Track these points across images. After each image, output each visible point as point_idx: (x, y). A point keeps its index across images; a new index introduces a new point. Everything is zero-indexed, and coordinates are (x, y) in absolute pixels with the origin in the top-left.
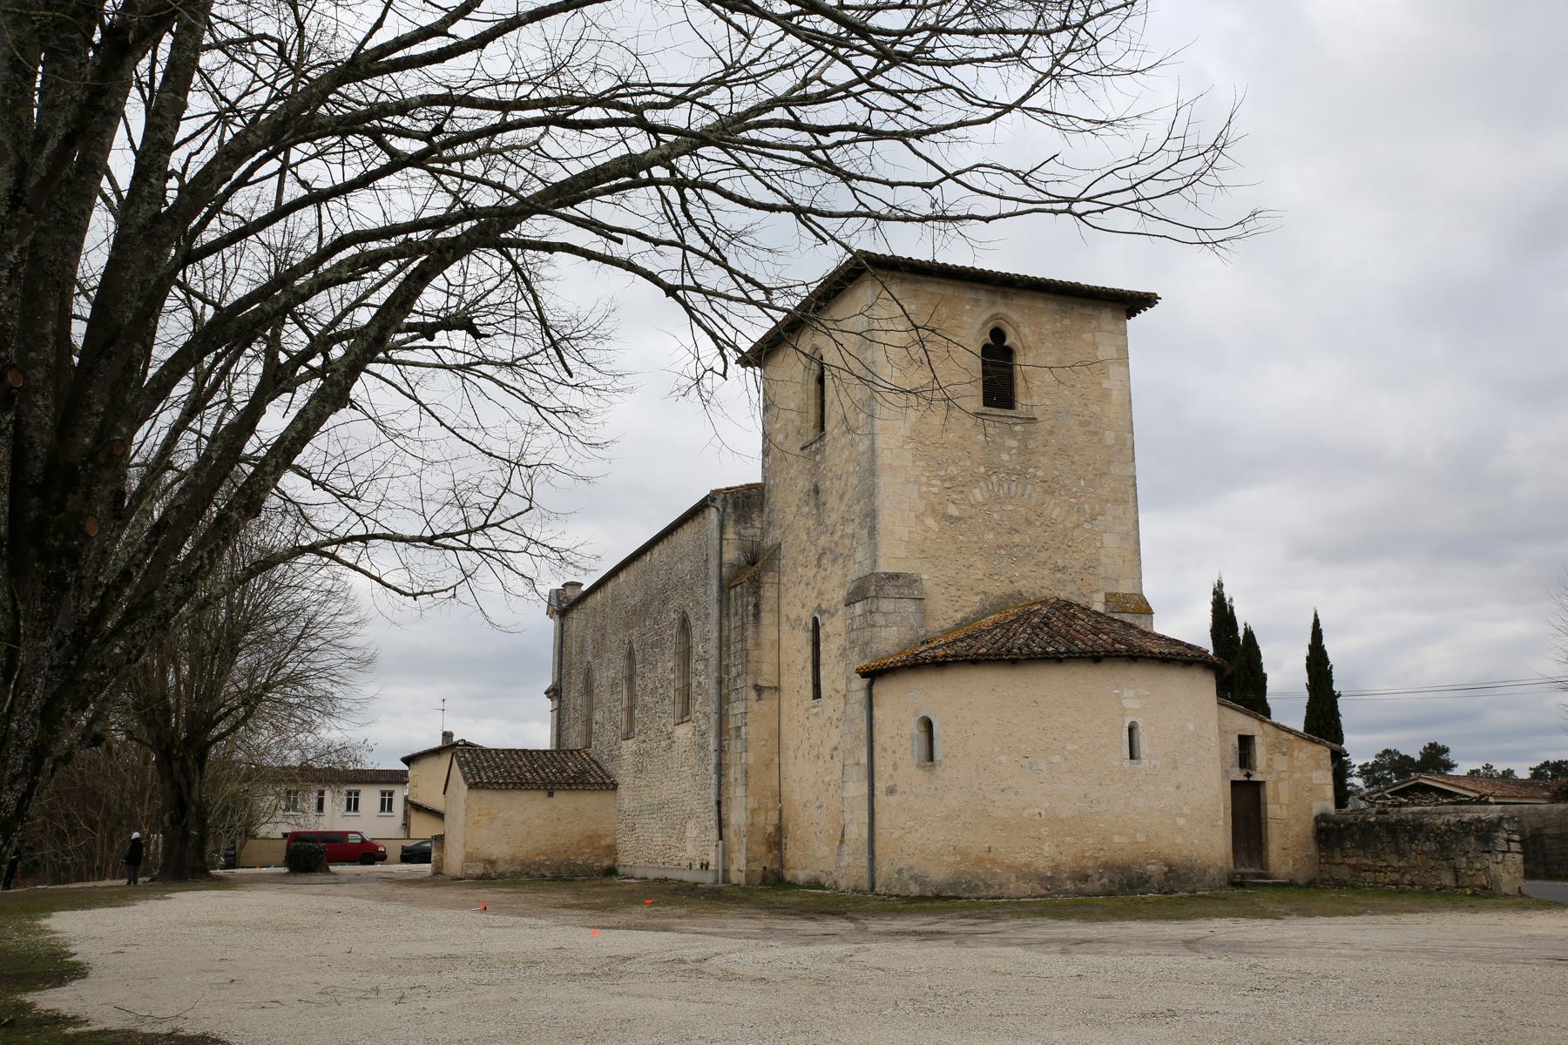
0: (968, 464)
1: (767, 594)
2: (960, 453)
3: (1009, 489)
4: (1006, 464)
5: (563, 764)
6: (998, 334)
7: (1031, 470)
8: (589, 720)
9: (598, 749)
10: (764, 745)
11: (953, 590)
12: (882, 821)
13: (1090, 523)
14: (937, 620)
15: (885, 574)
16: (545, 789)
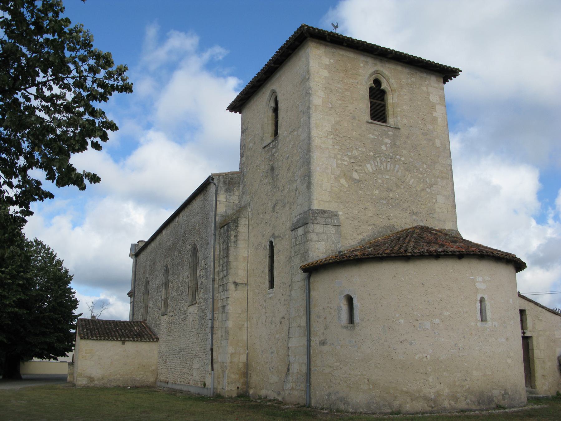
0: (364, 150)
1: (242, 230)
2: (359, 144)
3: (386, 167)
4: (385, 152)
5: (132, 328)
6: (377, 82)
7: (398, 157)
8: (146, 307)
9: (150, 321)
10: (239, 317)
11: (356, 222)
12: (317, 361)
13: (430, 188)
14: (347, 239)
15: (317, 210)
16: (121, 340)
